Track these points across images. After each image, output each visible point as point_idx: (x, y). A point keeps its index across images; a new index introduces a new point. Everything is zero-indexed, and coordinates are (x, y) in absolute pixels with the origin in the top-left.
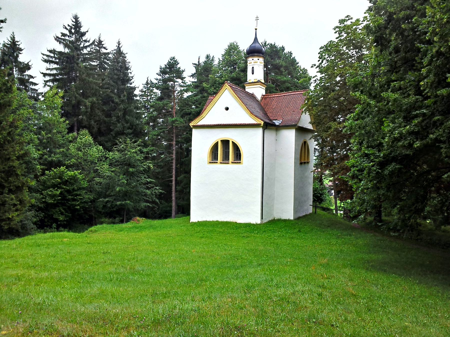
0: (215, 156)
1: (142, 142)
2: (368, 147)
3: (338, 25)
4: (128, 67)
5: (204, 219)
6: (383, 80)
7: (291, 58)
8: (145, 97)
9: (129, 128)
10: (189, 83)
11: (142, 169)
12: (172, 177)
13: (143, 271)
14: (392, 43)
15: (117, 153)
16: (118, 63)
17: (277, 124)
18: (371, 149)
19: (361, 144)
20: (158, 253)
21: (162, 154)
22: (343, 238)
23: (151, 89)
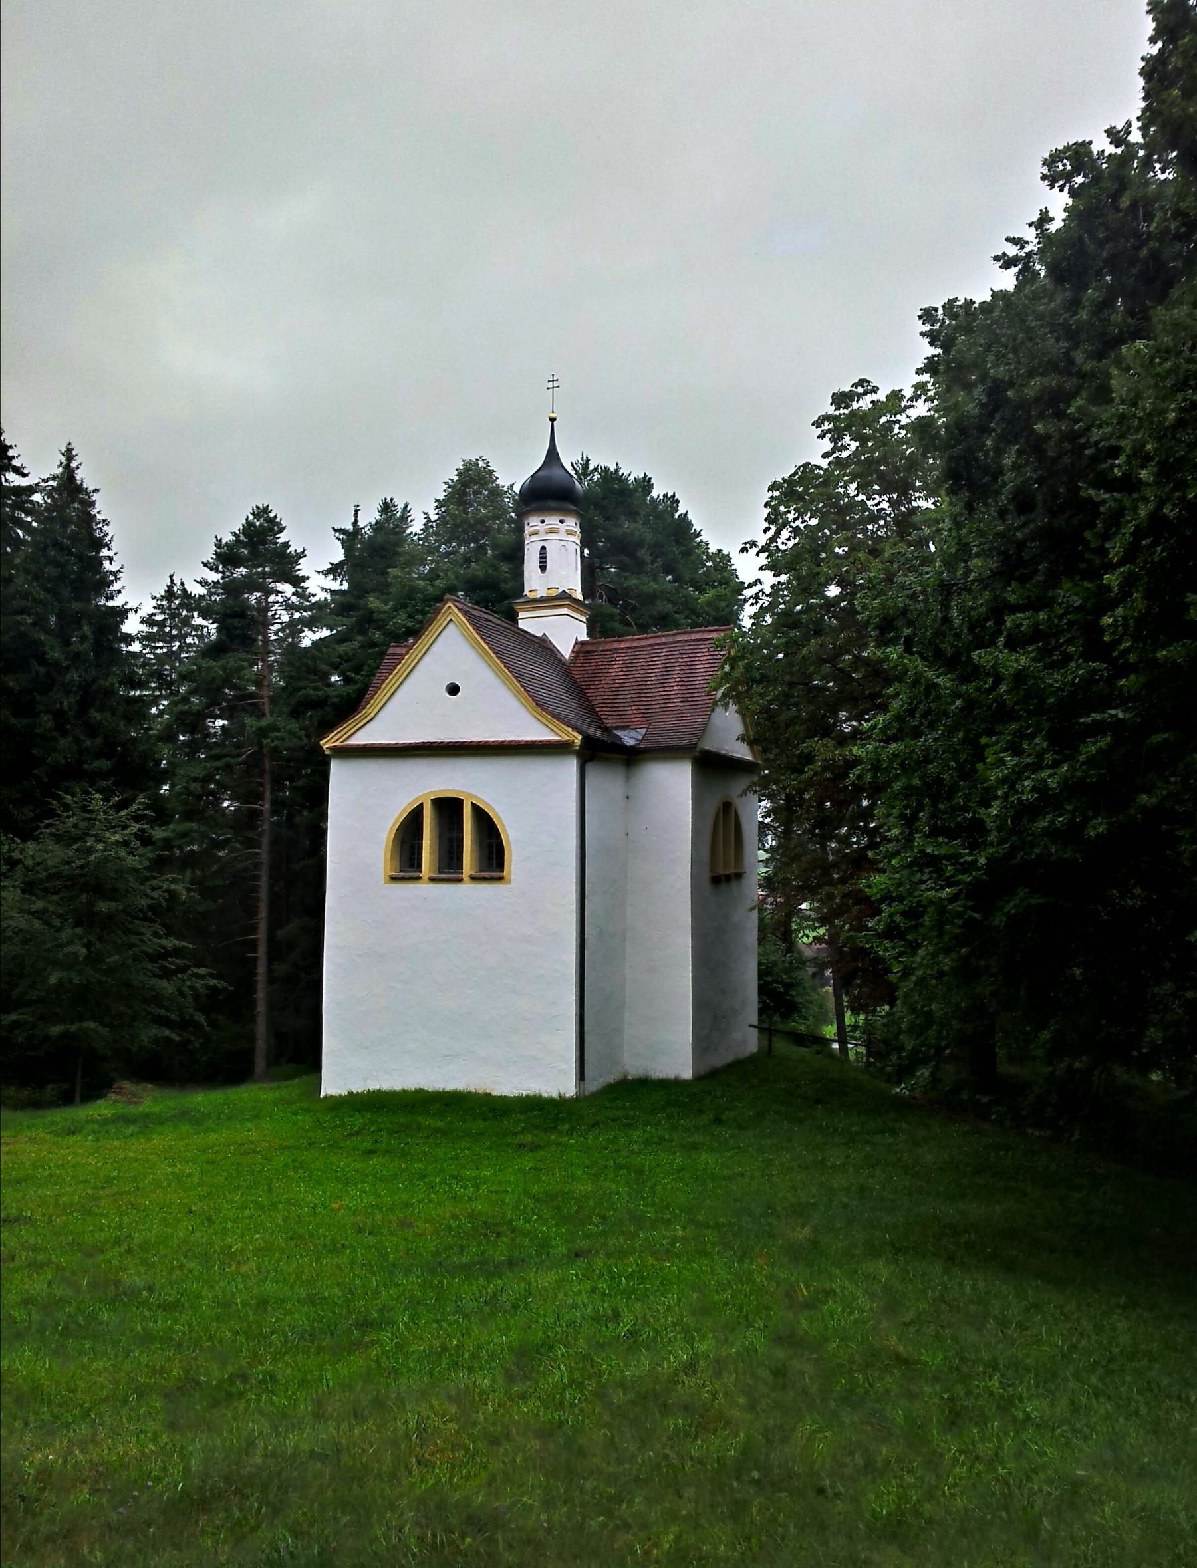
0: (413, 853)
1: (148, 807)
2: (935, 832)
3: (831, 410)
4: (102, 539)
5: (373, 1086)
6: (981, 602)
7: (676, 516)
8: (161, 644)
9: (99, 755)
10: (321, 596)
11: (144, 902)
12: (254, 929)
13: (150, 1289)
14: (1010, 475)
15: (51, 845)
16: (65, 523)
17: (630, 742)
18: (946, 840)
19: (910, 822)
20: (209, 1219)
21: (219, 845)
22: (867, 1142)
23: (184, 613)
